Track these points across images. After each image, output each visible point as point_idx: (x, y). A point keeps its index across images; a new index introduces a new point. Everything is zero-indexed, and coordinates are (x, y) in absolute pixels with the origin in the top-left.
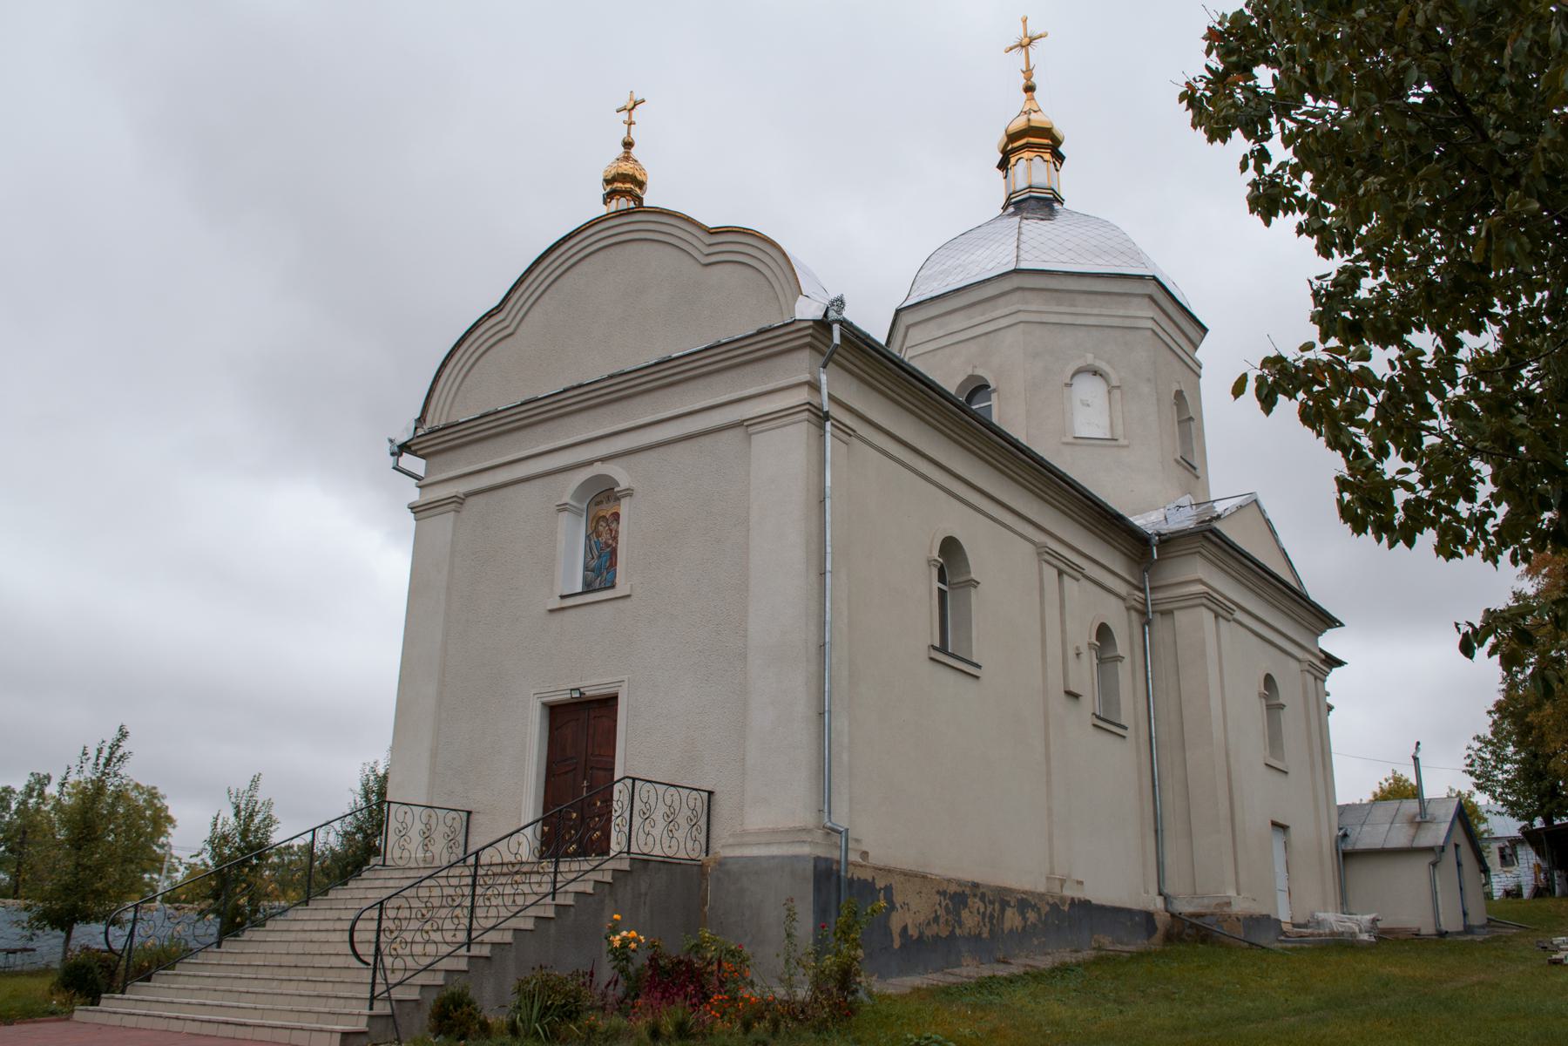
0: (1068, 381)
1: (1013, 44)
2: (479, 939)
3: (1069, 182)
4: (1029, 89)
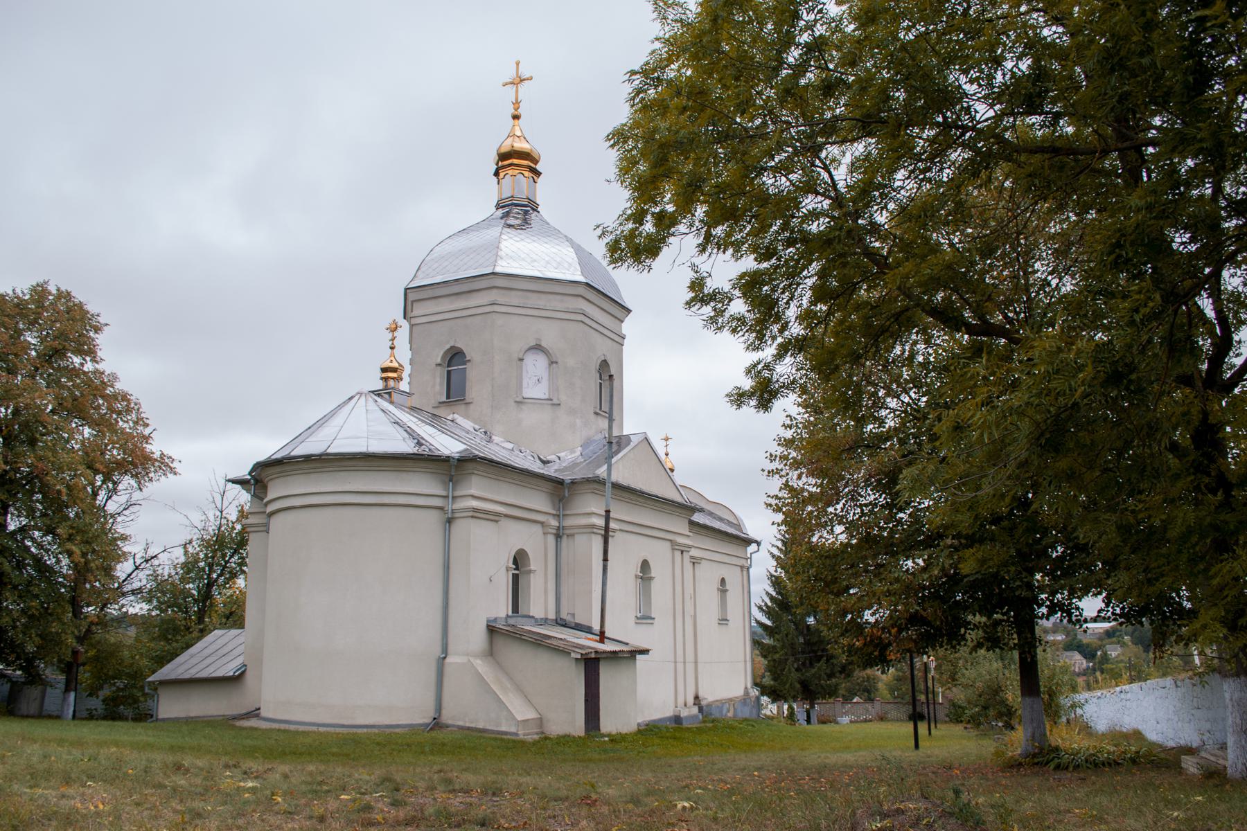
0: (521, 356)
1: (509, 80)
2: (983, 118)
3: (544, 192)
4: (516, 117)
